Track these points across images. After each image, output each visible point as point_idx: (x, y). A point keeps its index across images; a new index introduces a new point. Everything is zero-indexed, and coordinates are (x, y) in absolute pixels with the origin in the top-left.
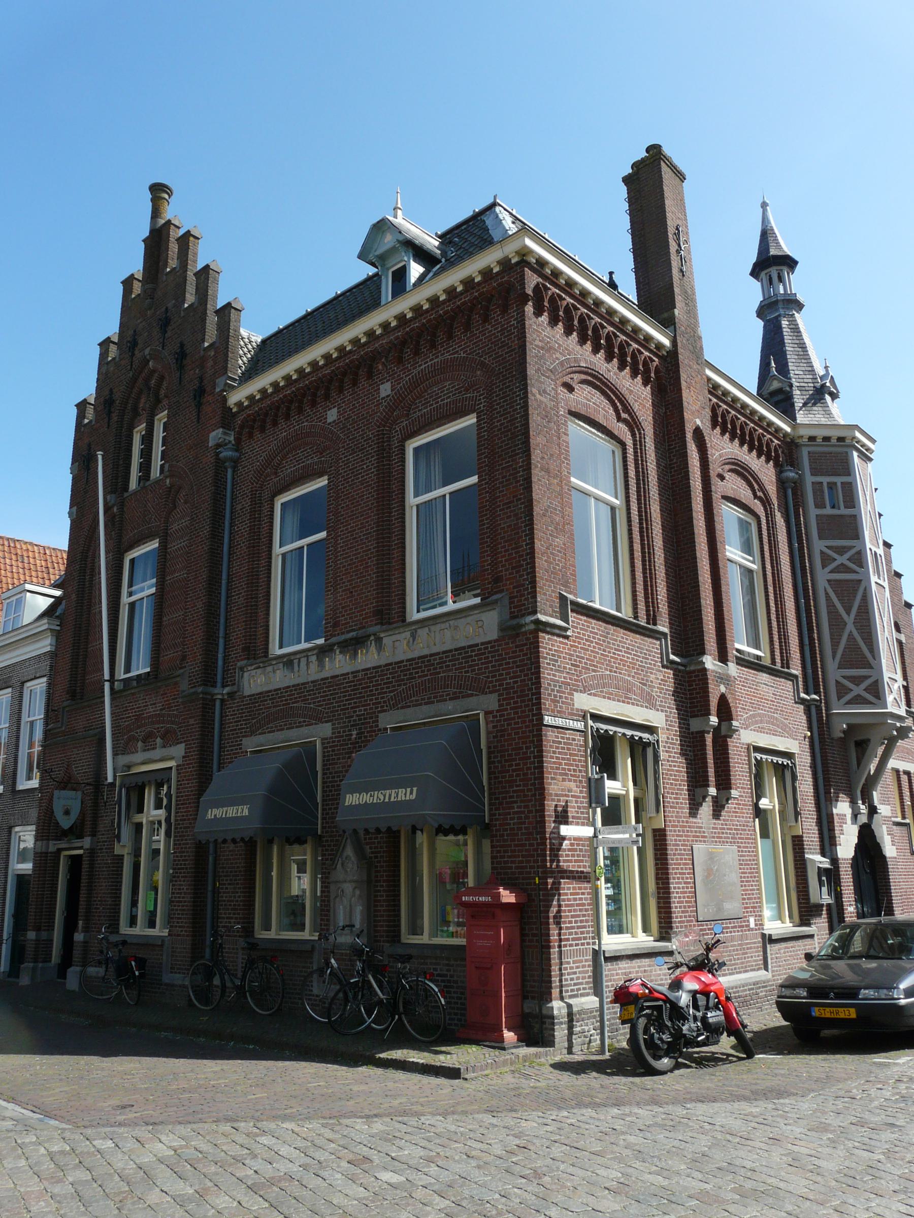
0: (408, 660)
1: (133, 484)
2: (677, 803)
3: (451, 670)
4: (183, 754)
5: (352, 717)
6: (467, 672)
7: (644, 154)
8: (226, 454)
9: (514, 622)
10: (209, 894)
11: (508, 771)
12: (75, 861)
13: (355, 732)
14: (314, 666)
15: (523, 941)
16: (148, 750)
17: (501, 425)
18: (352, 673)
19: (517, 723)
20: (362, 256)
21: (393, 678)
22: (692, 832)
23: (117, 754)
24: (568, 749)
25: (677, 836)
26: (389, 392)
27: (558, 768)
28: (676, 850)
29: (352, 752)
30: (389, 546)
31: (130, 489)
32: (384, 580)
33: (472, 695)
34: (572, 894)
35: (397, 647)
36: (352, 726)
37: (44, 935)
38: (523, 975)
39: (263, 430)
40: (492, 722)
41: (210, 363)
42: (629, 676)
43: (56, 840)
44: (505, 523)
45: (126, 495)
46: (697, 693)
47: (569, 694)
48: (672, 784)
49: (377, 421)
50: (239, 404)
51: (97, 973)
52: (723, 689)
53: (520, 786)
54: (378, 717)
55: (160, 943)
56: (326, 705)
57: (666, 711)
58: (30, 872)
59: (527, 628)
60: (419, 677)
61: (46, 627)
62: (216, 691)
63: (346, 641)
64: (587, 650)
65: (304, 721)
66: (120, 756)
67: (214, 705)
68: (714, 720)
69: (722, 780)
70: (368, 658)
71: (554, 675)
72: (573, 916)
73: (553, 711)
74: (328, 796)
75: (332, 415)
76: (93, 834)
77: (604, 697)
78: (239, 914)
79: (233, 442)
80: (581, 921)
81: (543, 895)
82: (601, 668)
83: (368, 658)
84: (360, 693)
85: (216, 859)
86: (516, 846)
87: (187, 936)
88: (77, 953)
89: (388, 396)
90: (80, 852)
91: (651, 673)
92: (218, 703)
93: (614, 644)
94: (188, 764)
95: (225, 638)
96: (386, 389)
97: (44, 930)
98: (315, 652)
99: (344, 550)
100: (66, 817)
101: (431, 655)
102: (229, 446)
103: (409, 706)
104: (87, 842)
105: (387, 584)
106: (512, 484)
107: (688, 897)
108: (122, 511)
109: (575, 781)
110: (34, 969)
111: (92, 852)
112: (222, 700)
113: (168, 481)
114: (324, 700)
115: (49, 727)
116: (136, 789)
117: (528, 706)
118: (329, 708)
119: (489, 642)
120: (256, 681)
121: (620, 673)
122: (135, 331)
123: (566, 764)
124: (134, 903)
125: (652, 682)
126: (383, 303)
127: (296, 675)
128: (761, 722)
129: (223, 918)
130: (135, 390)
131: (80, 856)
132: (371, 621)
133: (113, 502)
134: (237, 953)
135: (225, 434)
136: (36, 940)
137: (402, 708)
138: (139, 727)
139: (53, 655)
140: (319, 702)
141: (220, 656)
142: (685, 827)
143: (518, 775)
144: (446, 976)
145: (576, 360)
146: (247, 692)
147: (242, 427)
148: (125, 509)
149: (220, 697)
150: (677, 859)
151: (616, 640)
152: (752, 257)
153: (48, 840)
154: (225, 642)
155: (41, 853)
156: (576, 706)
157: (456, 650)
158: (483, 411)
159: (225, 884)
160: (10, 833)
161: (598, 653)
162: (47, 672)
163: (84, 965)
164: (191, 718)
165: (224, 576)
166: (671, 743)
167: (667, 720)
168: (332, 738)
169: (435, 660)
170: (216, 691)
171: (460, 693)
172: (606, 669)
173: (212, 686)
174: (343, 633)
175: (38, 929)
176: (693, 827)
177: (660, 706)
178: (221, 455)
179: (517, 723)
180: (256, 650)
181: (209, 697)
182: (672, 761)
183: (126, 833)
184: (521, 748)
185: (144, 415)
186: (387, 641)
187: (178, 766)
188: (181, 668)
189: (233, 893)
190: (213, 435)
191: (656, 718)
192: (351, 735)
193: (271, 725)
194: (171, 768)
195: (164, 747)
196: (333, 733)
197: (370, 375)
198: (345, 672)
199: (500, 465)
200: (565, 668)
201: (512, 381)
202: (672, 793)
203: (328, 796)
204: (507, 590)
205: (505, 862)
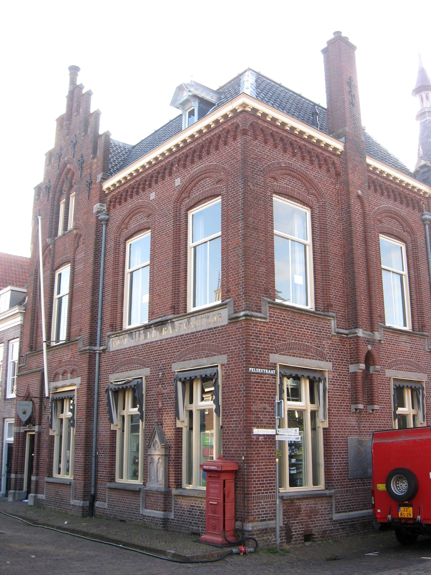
0: (186, 335)
1: (60, 232)
2: (338, 413)
3: (206, 341)
4: (80, 382)
5: (159, 365)
6: (213, 342)
7: (332, 36)
8: (102, 217)
9: (235, 315)
10: (94, 459)
11: (231, 398)
12: (32, 436)
13: (160, 374)
14: (142, 336)
15: (235, 490)
16: (65, 379)
17: (232, 203)
18: (160, 340)
19: (236, 371)
20: (173, 103)
21: (179, 344)
22: (348, 429)
23: (50, 382)
24: (265, 386)
25: (337, 432)
26: (179, 184)
27: (257, 397)
28: (336, 440)
29: (159, 385)
30: (179, 270)
31: (58, 235)
32: (175, 289)
33: (215, 355)
34: (264, 465)
35: (181, 328)
36: (160, 370)
37: (19, 476)
38: (236, 508)
39: (120, 204)
40: (224, 370)
41: (95, 166)
42: (308, 342)
43: (24, 426)
44: (232, 259)
45: (56, 238)
46: (354, 350)
47: (266, 355)
48: (335, 403)
49: (174, 199)
50: (108, 189)
51: (42, 497)
52: (370, 347)
53: (236, 406)
54: (171, 365)
55: (69, 483)
56: (148, 358)
57: (333, 361)
58: (13, 443)
59: (241, 319)
60: (191, 344)
61: (18, 311)
62: (96, 348)
63: (157, 323)
64: (280, 329)
65: (138, 367)
66: (52, 383)
67: (95, 356)
68: (363, 366)
69: (370, 399)
70: (168, 332)
71: (256, 345)
72: (264, 478)
73: (255, 365)
74: (148, 408)
75: (153, 196)
76: (40, 424)
77: (290, 355)
78: (107, 470)
79: (106, 210)
80: (270, 480)
81: (247, 466)
82: (289, 339)
83: (168, 332)
84: (164, 352)
85: (97, 440)
86: (234, 439)
87: (82, 480)
88: (33, 486)
89: (179, 186)
90: (34, 433)
91: (324, 340)
92: (97, 355)
93: (298, 325)
94: (82, 388)
95: (101, 319)
96: (178, 182)
97: (19, 474)
98: (142, 329)
99: (157, 272)
100: (24, 415)
101: (197, 332)
102: (104, 212)
103: (186, 360)
104: (36, 428)
105: (177, 291)
106: (236, 237)
107: (343, 466)
108: (54, 248)
109: (269, 403)
110: (14, 494)
111: (39, 433)
112: (100, 354)
113: (75, 231)
114: (147, 355)
115: (21, 365)
116: (59, 401)
117: (241, 362)
118: (149, 360)
119: (224, 326)
120: (116, 344)
121: (302, 341)
122: (61, 147)
123: (263, 394)
124: (60, 462)
125: (324, 345)
126: (183, 129)
127: (134, 341)
128: (401, 364)
129: (100, 471)
130: (61, 180)
131: (34, 435)
132: (169, 312)
133: (49, 242)
134: (106, 490)
135: (101, 205)
136: (15, 479)
137: (183, 361)
138: (61, 367)
139: (22, 326)
140: (144, 356)
141: (99, 329)
142: (344, 426)
143: (236, 400)
144: (200, 507)
145: (279, 163)
146: (111, 350)
147: (110, 202)
148: (56, 247)
149: (98, 352)
150: (337, 445)
151: (300, 323)
152: (413, 84)
153: (20, 426)
154: (102, 321)
155: (17, 433)
156: (271, 361)
157: (209, 329)
158: (224, 195)
159: (100, 453)
160: (4, 421)
161: (287, 331)
162: (19, 335)
163: (36, 492)
164: (83, 363)
165: (101, 285)
166: (335, 380)
167: (333, 367)
168: (150, 376)
169: (198, 335)
170: (96, 348)
171: (210, 353)
172: (293, 340)
173: (94, 346)
174: (156, 318)
175: (16, 473)
176: (349, 427)
177: (329, 358)
178: (99, 218)
179: (236, 371)
180: (116, 327)
181: (92, 352)
182: (336, 390)
183: (55, 424)
184: (238, 385)
185: (64, 196)
186: (177, 323)
187: (78, 389)
188: (79, 336)
189: (104, 458)
190: (95, 206)
191: (326, 366)
192: (159, 375)
193: (122, 368)
194: (74, 390)
195: (72, 378)
196: (151, 374)
197: (170, 174)
198: (156, 340)
199: (231, 226)
200: (264, 340)
201: (237, 179)
202: (335, 408)
203: (148, 408)
204: (233, 297)
205: (229, 448)
